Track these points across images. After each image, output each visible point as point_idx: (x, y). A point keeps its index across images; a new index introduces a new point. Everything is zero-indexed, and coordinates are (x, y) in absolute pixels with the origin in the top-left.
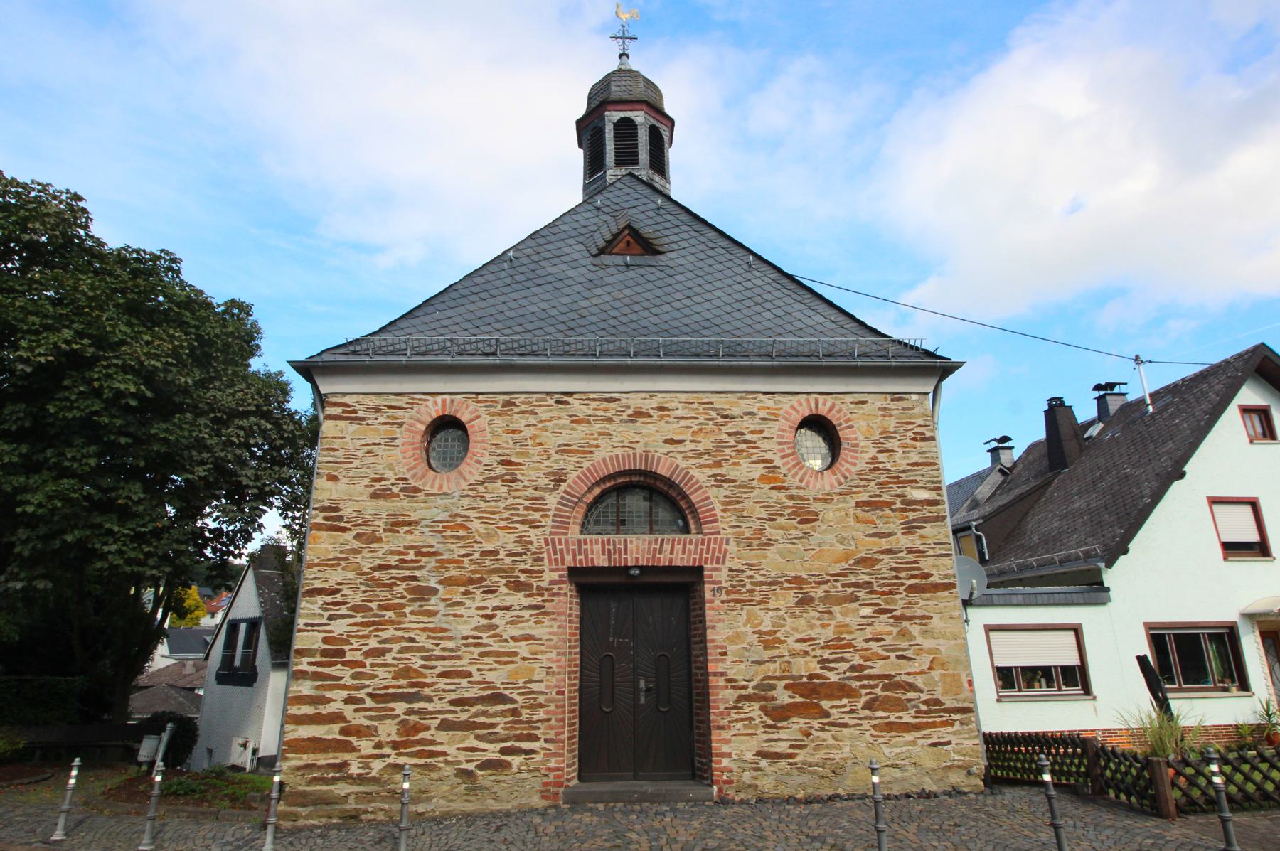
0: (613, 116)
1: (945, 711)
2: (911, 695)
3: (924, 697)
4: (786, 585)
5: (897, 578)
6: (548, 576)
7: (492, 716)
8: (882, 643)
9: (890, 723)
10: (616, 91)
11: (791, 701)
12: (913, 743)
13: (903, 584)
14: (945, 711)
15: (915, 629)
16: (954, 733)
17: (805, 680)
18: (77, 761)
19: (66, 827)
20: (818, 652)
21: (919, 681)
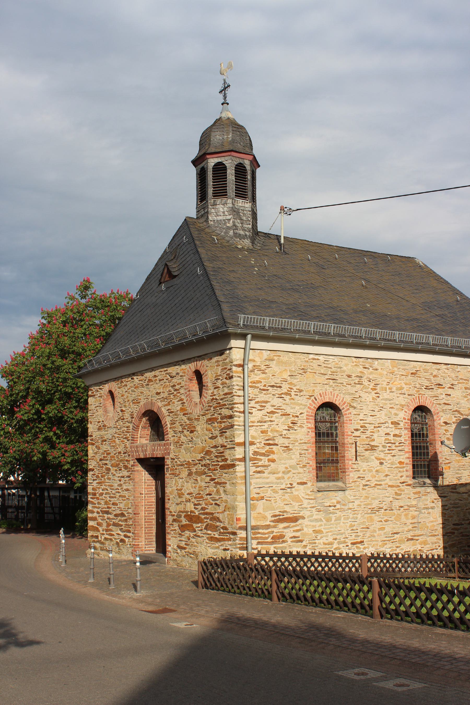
0: (212, 162)
1: (229, 533)
2: (218, 524)
3: (222, 525)
4: (186, 466)
5: (218, 461)
6: (132, 463)
7: (265, 534)
8: (211, 496)
9: (211, 537)
10: (217, 138)
11: (186, 523)
12: (218, 548)
13: (218, 465)
14: (229, 533)
15: (221, 490)
16: (230, 545)
17: (189, 513)
18: (62, 531)
19: (398, 616)
20: (193, 500)
21: (221, 516)
